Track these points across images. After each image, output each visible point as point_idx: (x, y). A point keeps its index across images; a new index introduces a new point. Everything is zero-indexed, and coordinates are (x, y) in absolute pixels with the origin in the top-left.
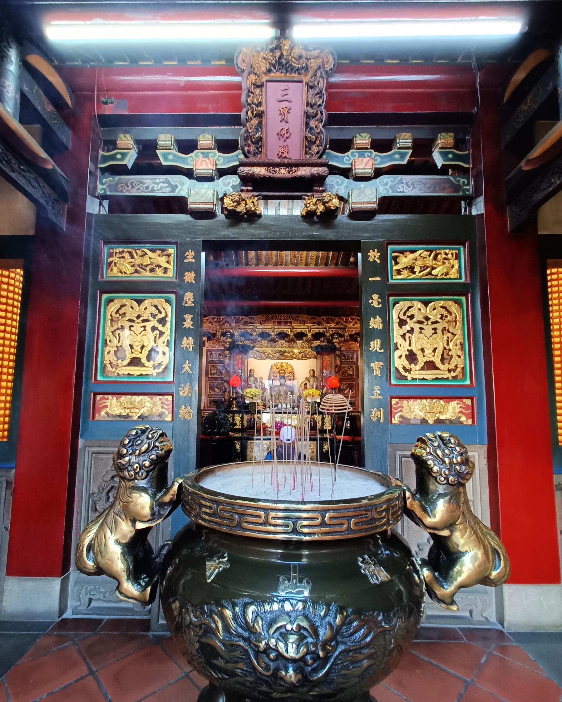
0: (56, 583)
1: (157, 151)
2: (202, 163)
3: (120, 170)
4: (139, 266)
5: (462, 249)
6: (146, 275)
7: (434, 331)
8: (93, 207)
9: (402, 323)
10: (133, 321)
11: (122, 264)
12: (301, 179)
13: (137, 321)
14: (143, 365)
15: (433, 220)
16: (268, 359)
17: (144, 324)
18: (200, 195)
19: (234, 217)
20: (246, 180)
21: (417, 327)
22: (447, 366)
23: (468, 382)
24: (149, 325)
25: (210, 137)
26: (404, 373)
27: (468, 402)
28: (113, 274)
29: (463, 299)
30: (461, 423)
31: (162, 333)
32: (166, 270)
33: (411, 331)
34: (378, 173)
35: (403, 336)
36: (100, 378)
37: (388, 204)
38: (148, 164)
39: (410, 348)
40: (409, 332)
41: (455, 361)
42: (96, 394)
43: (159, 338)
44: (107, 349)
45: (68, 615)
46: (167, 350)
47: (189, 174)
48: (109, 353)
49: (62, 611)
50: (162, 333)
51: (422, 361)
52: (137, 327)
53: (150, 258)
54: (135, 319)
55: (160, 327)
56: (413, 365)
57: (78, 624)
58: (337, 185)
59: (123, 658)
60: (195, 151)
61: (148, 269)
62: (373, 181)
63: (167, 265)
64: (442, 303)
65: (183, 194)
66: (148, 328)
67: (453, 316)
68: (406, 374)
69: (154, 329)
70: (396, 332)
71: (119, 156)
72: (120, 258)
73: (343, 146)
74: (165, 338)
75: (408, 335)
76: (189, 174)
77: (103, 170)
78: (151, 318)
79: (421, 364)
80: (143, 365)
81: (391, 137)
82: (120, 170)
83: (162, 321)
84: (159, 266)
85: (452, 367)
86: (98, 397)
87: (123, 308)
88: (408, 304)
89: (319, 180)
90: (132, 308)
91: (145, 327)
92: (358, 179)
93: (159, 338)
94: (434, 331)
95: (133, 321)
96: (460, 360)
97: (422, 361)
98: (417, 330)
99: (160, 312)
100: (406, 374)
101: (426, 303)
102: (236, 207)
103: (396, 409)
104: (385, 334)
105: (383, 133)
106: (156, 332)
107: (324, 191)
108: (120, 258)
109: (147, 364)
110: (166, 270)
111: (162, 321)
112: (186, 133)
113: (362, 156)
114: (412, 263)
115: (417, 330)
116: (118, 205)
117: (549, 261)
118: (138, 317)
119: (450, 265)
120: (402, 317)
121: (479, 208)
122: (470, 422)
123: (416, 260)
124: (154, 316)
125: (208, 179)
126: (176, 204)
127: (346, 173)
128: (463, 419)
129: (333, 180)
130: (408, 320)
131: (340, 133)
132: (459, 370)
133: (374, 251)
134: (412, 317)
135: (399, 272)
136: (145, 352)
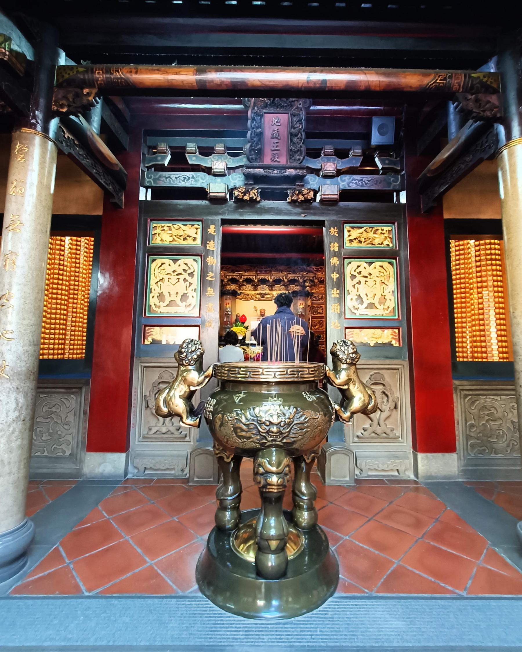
0: (123, 455)
1: (186, 154)
2: (218, 164)
3: (161, 168)
4: (175, 236)
5: (394, 227)
6: (180, 243)
7: (177, 280)
8: (144, 195)
9: (353, 277)
10: (366, 277)
11: (163, 234)
12: (288, 177)
13: (369, 277)
14: (178, 306)
15: (372, 206)
16: (252, 301)
17: (178, 277)
18: (217, 187)
19: (240, 203)
20: (247, 177)
21: (363, 280)
22: (184, 303)
23: (397, 317)
24: (181, 277)
25: (223, 145)
26: (354, 311)
27: (397, 331)
28: (157, 241)
29: (394, 261)
30: (392, 345)
31: (191, 284)
32: (195, 239)
33: (359, 283)
34: (339, 173)
35: (354, 286)
36: (147, 315)
37: (346, 195)
38: (180, 162)
39: (358, 294)
40: (357, 283)
41: (388, 303)
42: (145, 326)
43: (189, 287)
44: (151, 295)
45: (129, 476)
46: (194, 294)
47: (208, 171)
48: (153, 297)
49: (126, 473)
50: (191, 284)
51: (168, 300)
52: (370, 281)
53: (184, 231)
54: (172, 273)
55: (189, 278)
56: (161, 303)
57: (135, 481)
58: (313, 181)
59: (340, 497)
60: (213, 155)
61: (182, 238)
62: (336, 178)
63: (195, 236)
64: (380, 264)
65: (204, 186)
66: (181, 280)
67: (388, 273)
68: (355, 311)
69: (185, 280)
70: (349, 283)
71: (159, 158)
72: (162, 230)
73: (315, 154)
74: (193, 287)
75: (357, 286)
76: (208, 171)
77: (149, 168)
78: (183, 273)
79: (167, 302)
80: (178, 306)
81: (319, 147)
82: (161, 168)
83: (191, 274)
84: (189, 236)
85: (158, 304)
86: (147, 328)
87: (163, 265)
88: (358, 263)
89: (301, 178)
90: (169, 265)
91: (178, 279)
92: (326, 176)
93: (189, 287)
94: (177, 280)
95: (366, 277)
96: (392, 302)
97: (168, 300)
98: (363, 282)
99: (189, 268)
100: (355, 311)
101: (175, 261)
102: (243, 196)
103: (349, 336)
104: (340, 284)
105: (342, 143)
106: (187, 284)
107: (303, 186)
108: (162, 230)
109: (378, 306)
110: (195, 239)
111: (191, 274)
112: (207, 142)
113: (328, 161)
114: (355, 236)
115: (363, 282)
116: (159, 193)
117: (451, 235)
118: (174, 271)
119: (382, 236)
120: (353, 273)
121: (403, 198)
122: (397, 345)
123: (362, 233)
124: (185, 271)
125: (221, 175)
126: (200, 193)
127: (316, 172)
128: (394, 342)
129: (310, 178)
130: (357, 275)
131: (315, 143)
132: (390, 310)
133: (334, 228)
134: (360, 273)
135: (351, 241)
136: (179, 296)
